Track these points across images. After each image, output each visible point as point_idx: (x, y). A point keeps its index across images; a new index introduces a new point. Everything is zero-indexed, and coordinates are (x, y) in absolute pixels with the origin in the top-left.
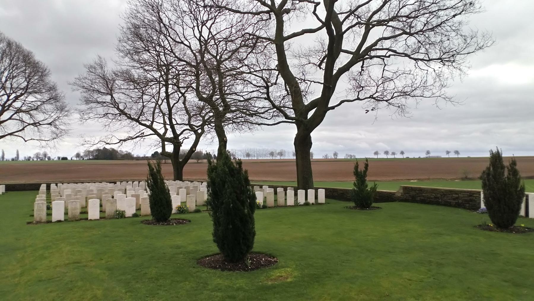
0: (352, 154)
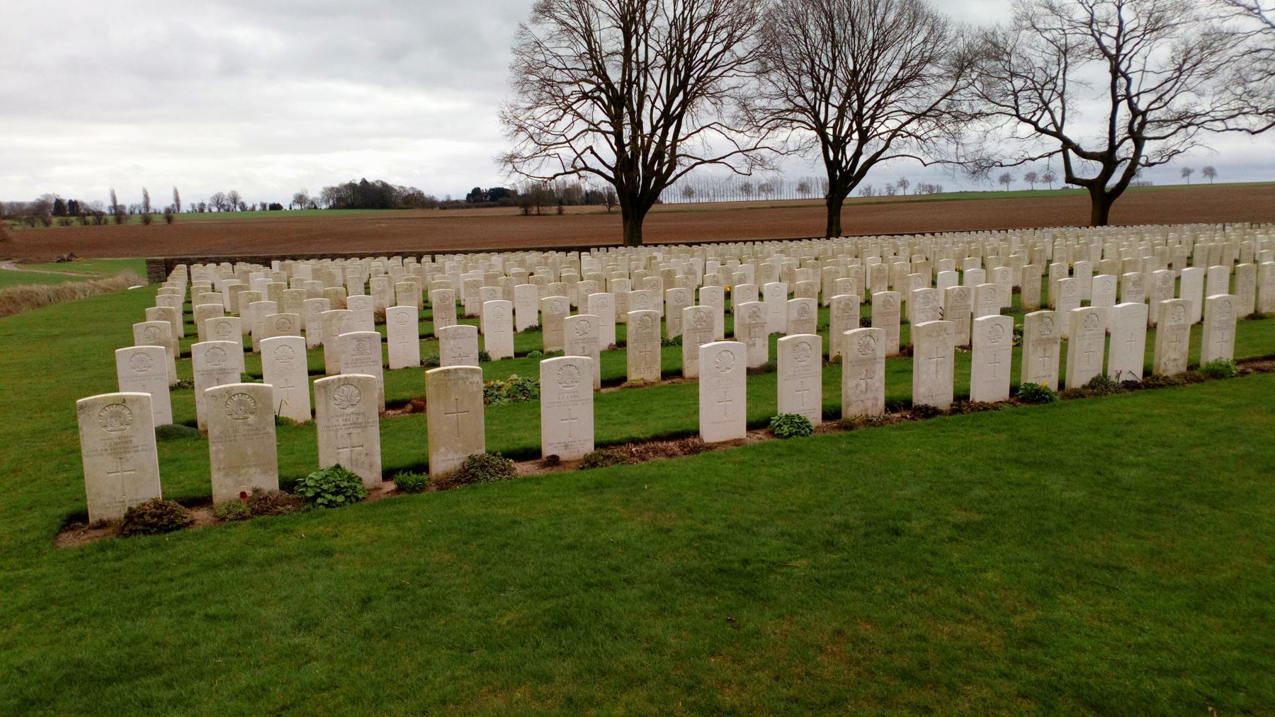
0: (934, 184)
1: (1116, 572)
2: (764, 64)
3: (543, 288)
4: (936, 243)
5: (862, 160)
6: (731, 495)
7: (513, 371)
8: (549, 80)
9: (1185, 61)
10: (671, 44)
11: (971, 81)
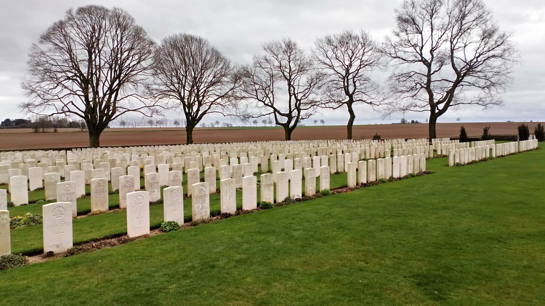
0: (229, 123)
1: (292, 271)
2: (156, 71)
3: (45, 169)
4: (230, 147)
5: (200, 113)
6: (142, 260)
7: (28, 211)
8: (49, 70)
9: (311, 83)
10: (112, 59)
11: (240, 85)
